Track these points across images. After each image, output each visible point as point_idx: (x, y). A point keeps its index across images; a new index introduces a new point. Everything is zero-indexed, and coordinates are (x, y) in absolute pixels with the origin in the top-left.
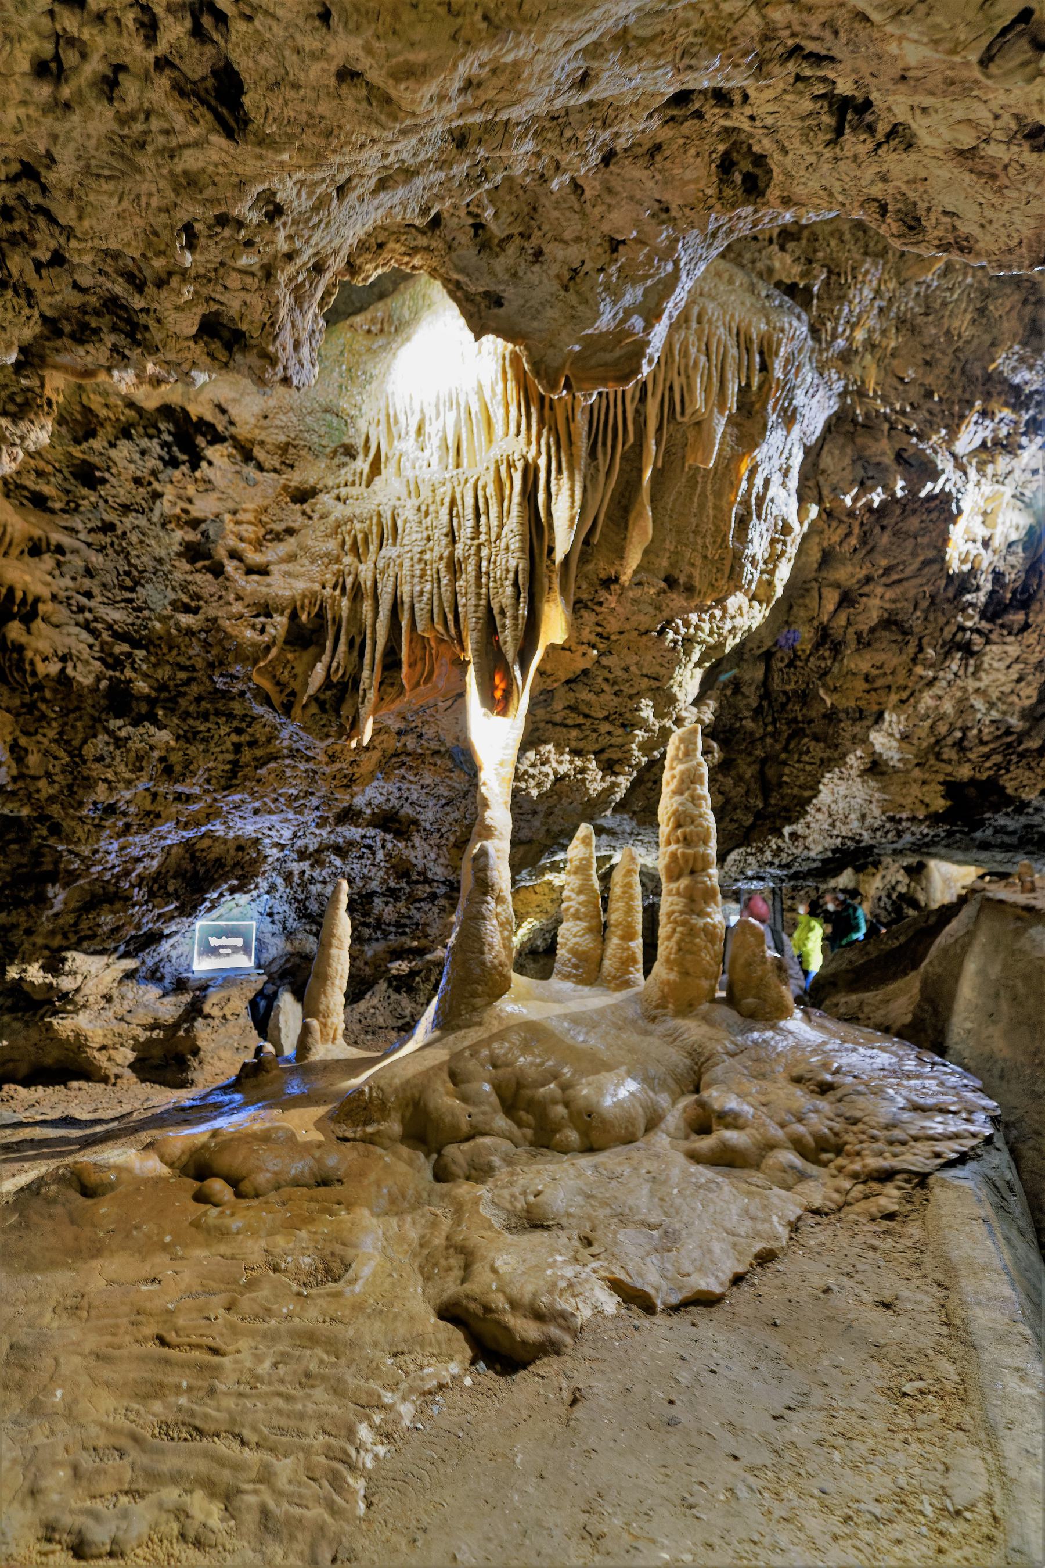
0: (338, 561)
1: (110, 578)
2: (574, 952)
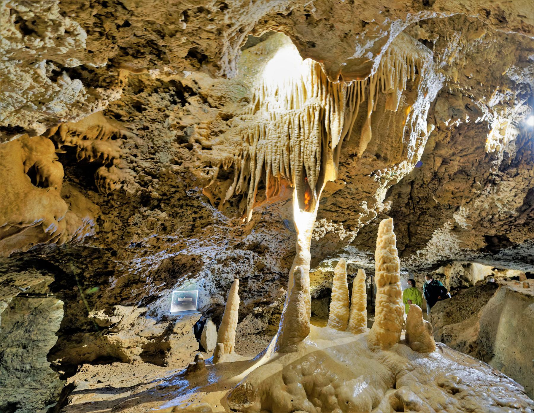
0: (241, 145)
1: (145, 149)
2: (338, 316)
